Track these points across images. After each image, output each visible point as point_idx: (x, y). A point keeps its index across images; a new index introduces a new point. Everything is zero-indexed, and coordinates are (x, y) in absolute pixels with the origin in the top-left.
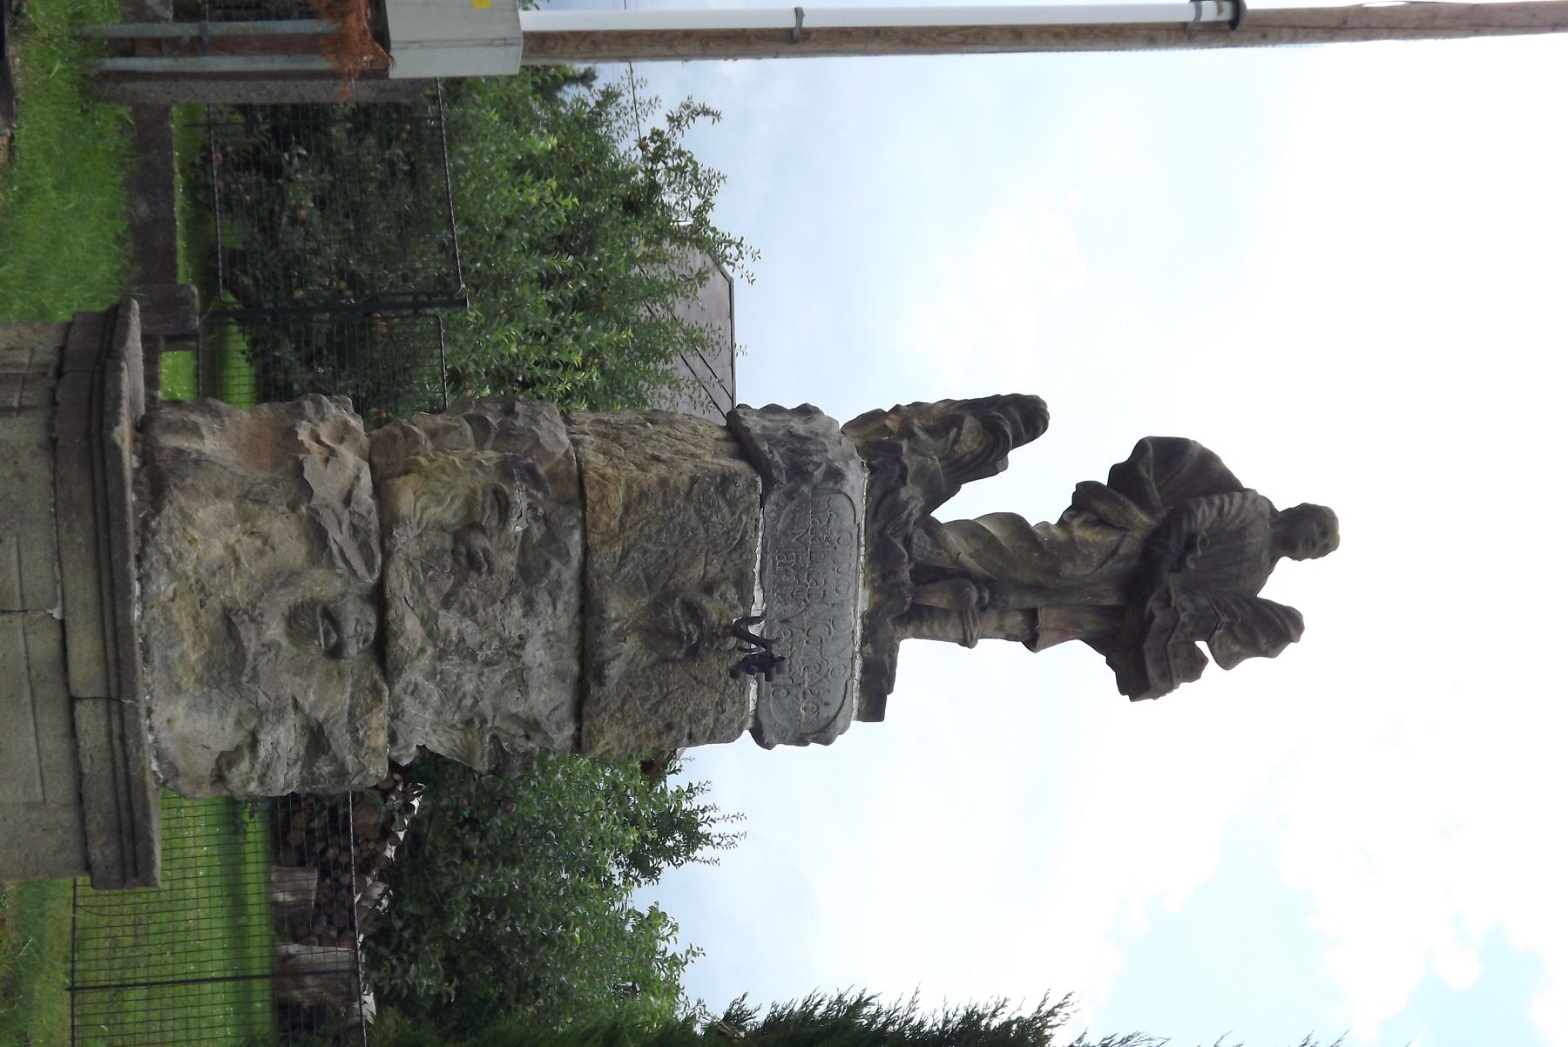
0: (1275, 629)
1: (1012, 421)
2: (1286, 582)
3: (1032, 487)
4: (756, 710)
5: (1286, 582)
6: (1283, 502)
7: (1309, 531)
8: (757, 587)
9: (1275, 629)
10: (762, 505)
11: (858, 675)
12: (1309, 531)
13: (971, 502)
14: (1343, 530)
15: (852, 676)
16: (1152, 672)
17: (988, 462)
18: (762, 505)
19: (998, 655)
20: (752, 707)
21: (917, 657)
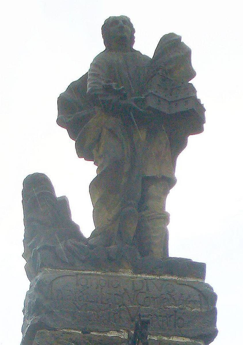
0: (172, 48)
1: (38, 193)
2: (146, 45)
3: (75, 179)
4: (191, 338)
5: (146, 45)
6: (99, 46)
7: (118, 32)
8: (109, 335)
9: (172, 48)
10: (55, 330)
11: (174, 278)
12: (118, 32)
13: (84, 217)
14: (117, 14)
15: (175, 281)
16: (182, 108)
17: (62, 206)
18: (55, 330)
19: (174, 202)
20: (187, 340)
21: (176, 250)
